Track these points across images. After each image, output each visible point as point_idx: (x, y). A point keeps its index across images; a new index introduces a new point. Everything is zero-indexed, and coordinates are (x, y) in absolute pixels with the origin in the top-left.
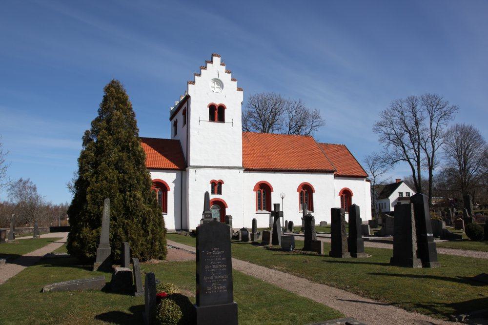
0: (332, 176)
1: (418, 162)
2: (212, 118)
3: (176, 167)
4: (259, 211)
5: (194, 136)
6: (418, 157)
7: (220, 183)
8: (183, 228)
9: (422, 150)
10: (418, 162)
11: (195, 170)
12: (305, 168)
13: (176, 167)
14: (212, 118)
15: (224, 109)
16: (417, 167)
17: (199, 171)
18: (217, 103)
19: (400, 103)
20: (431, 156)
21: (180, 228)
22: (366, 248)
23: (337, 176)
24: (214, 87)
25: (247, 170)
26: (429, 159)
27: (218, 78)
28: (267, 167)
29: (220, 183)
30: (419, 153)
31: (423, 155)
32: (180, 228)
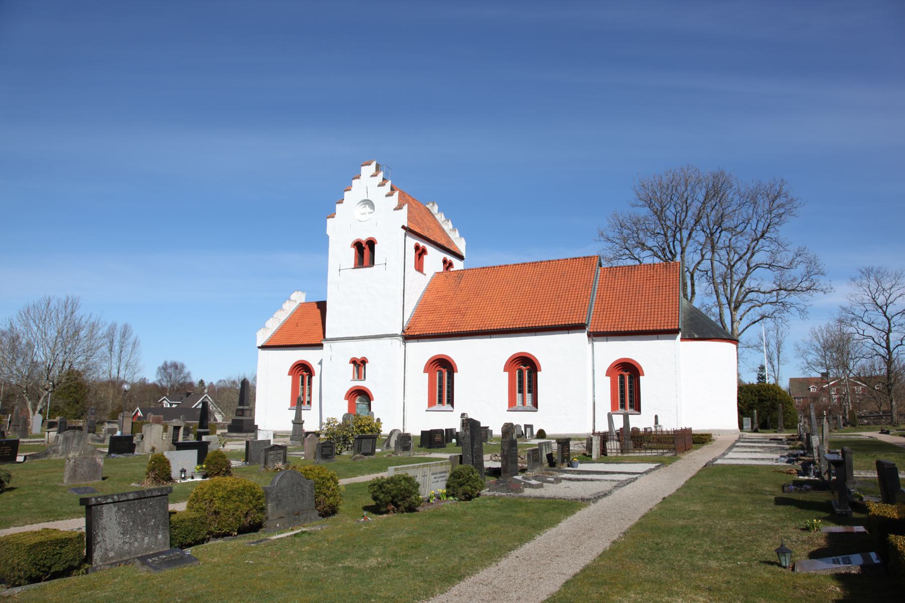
0: (582, 336)
11: (330, 344)
23: (594, 336)
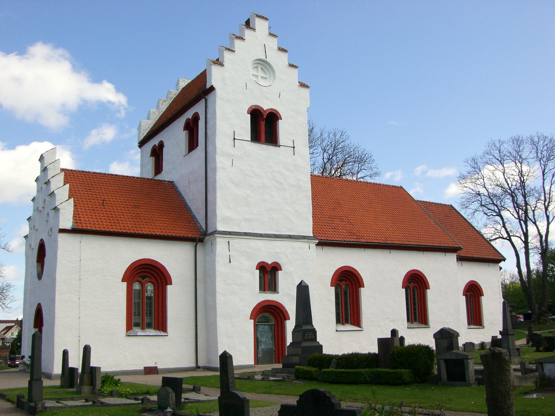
0: (453, 257)
1: (526, 242)
2: (256, 137)
3: (524, 240)
4: (341, 327)
5: (224, 169)
6: (526, 235)
7: (276, 268)
8: (200, 364)
9: (530, 224)
10: (526, 242)
11: (227, 240)
12: (413, 243)
13: (524, 240)
14: (256, 137)
15: (278, 119)
16: (524, 250)
17: (236, 242)
18: (266, 106)
19: (498, 145)
20: (543, 233)
21: (194, 365)
22: (102, 371)
23: (461, 259)
24: (257, 76)
25: (321, 244)
26: (541, 236)
27: (264, 58)
28: (353, 239)
29: (276, 268)
30: (526, 226)
31: (532, 229)
32: (194, 365)
